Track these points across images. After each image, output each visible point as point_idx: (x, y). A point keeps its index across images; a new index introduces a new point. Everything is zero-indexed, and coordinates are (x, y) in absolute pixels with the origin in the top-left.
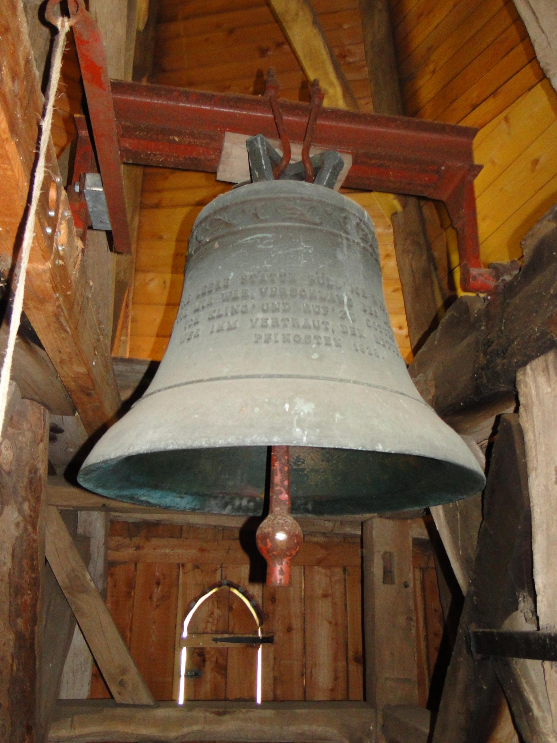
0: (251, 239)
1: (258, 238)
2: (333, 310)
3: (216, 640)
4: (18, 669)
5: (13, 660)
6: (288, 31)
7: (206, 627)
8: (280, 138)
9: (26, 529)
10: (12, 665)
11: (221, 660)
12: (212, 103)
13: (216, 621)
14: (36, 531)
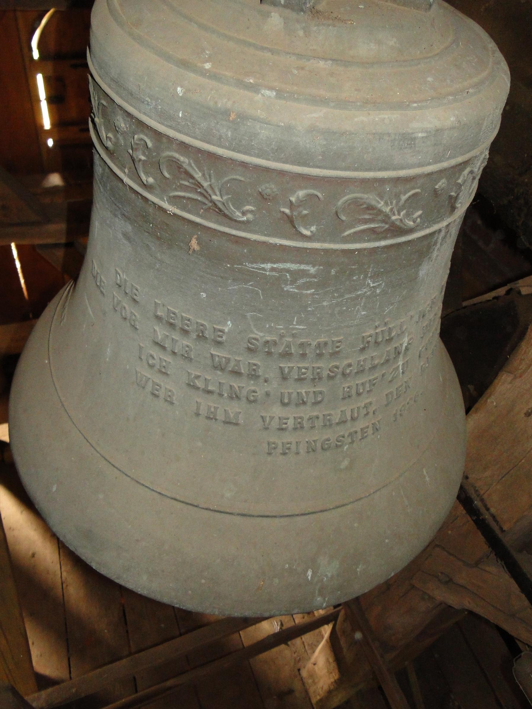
0: (273, 269)
1: (288, 271)
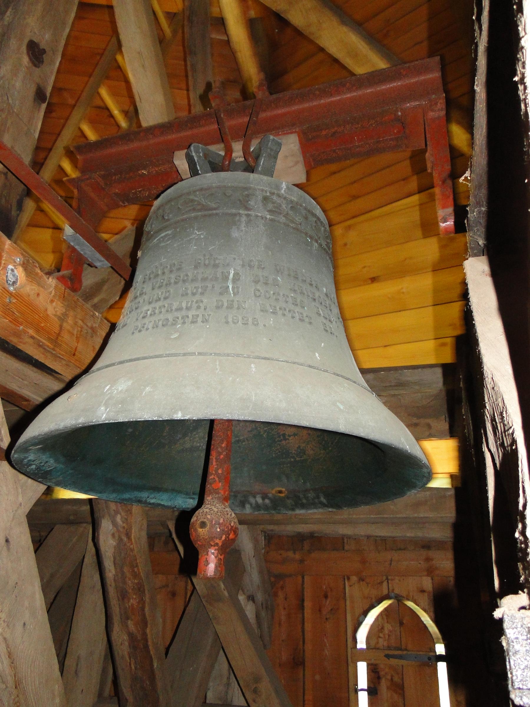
2: (213, 287)
3: (388, 656)
4: (136, 668)
5: (130, 659)
6: (317, 42)
7: (378, 643)
8: (223, 141)
9: (120, 540)
10: (130, 664)
11: (396, 679)
12: (174, 131)
13: (387, 637)
14: (131, 540)
